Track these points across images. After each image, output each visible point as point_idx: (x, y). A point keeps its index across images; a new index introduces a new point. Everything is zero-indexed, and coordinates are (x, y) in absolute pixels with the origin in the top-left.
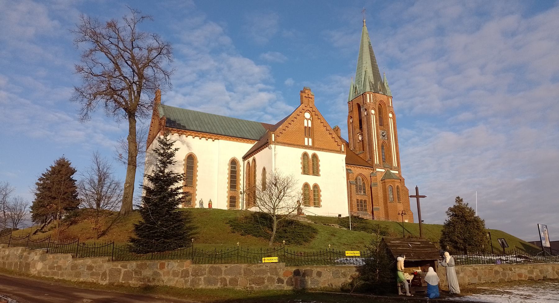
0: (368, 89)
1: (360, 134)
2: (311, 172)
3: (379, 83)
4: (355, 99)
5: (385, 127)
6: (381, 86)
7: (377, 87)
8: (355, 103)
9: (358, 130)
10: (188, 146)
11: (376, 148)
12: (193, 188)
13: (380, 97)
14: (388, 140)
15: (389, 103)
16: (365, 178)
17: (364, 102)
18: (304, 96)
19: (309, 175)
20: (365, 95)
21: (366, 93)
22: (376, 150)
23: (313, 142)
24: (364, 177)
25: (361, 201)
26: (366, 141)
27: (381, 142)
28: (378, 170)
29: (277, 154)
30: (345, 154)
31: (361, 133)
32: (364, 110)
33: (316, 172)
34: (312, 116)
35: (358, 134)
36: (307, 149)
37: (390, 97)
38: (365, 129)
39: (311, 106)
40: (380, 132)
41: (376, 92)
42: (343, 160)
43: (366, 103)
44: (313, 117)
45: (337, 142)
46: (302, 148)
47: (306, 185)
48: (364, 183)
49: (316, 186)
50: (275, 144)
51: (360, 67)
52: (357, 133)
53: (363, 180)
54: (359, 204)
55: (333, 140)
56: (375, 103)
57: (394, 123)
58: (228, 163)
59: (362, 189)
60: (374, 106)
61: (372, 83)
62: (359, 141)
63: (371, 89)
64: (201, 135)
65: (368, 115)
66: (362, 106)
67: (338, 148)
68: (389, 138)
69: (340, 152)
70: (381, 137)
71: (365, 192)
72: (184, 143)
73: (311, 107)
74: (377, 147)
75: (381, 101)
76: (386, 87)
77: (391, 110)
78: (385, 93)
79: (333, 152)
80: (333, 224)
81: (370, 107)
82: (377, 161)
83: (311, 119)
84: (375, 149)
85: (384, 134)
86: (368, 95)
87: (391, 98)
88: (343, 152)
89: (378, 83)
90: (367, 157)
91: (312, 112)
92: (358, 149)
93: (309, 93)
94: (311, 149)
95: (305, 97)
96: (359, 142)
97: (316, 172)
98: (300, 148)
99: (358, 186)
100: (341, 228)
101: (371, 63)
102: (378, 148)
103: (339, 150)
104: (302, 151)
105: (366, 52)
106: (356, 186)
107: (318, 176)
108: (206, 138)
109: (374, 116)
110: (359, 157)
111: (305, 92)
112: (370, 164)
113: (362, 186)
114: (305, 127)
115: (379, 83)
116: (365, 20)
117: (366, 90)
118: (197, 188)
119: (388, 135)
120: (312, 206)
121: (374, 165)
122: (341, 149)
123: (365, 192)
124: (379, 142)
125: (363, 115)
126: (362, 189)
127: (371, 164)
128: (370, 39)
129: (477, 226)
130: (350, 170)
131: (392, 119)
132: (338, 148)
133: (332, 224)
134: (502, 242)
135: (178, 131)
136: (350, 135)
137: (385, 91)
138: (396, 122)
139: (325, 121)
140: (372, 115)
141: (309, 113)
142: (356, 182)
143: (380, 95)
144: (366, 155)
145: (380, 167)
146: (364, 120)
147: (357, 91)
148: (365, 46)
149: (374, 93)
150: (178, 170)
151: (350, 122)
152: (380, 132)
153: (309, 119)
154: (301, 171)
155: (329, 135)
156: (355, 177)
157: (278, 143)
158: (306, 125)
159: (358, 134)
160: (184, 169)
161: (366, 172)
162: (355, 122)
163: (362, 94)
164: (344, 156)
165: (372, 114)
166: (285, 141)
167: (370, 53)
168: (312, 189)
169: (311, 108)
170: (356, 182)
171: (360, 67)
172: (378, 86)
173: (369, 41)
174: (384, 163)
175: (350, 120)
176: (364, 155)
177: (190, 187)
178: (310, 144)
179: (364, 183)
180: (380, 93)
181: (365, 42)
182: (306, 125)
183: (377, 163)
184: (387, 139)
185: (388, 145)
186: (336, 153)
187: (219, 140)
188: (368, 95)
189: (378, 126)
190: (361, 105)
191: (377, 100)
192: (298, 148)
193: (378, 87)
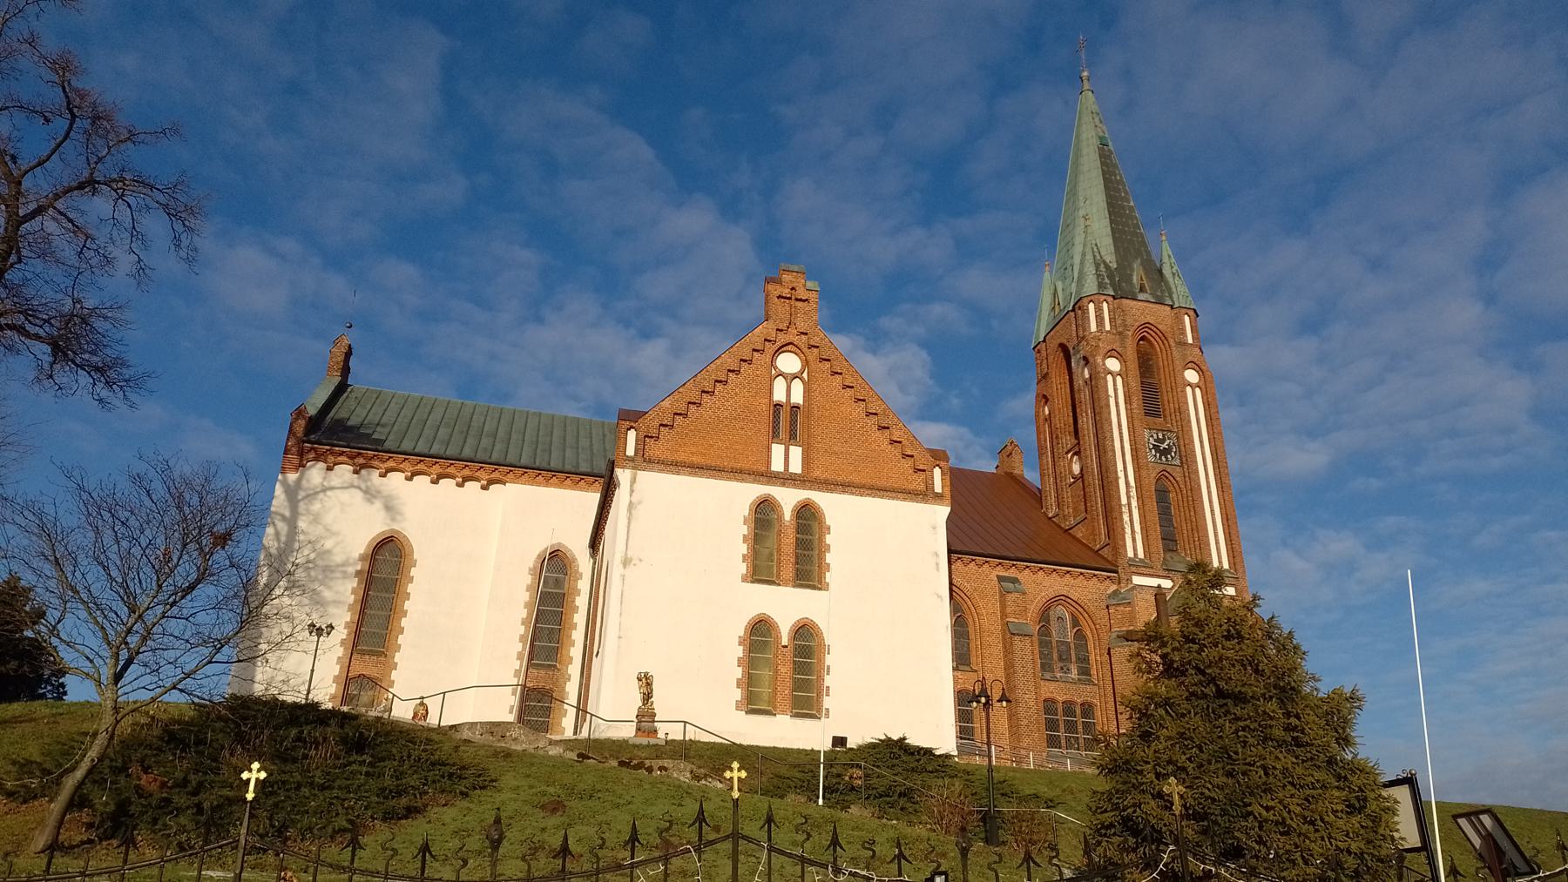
0: (1091, 286)
1: (1075, 454)
2: (788, 571)
3: (1137, 265)
4: (1052, 333)
5: (1168, 419)
6: (1145, 274)
7: (1129, 279)
8: (1053, 344)
9: (1068, 441)
10: (389, 508)
11: (1129, 497)
12: (382, 659)
13: (1141, 310)
14: (1182, 466)
15: (1183, 333)
16: (1086, 615)
17: (1081, 334)
18: (777, 293)
19: (779, 585)
20: (1080, 308)
21: (1085, 300)
22: (1129, 504)
23: (806, 461)
24: (1080, 609)
25: (1069, 708)
26: (1094, 479)
27: (1151, 476)
28: (1137, 580)
29: (640, 503)
30: (948, 502)
31: (1077, 449)
32: (1082, 362)
33: (808, 571)
34: (806, 363)
35: (1069, 455)
36: (774, 484)
37: (1184, 311)
38: (1088, 430)
39: (802, 326)
40: (1149, 438)
41: (1122, 292)
42: (934, 528)
43: (1083, 338)
44: (813, 366)
45: (912, 456)
46: (754, 481)
47: (760, 629)
48: (1080, 635)
49: (805, 632)
50: (634, 468)
51: (1069, 221)
52: (1065, 450)
53: (1075, 622)
54: (1061, 717)
55: (896, 451)
56: (1120, 333)
57: (1208, 405)
58: (531, 566)
59: (1073, 659)
60: (1118, 344)
61: (1107, 266)
62: (1072, 480)
63: (1101, 285)
64: (436, 469)
65: (1096, 384)
66: (1074, 348)
67: (917, 483)
68: (1187, 460)
69: (925, 495)
70: (1151, 456)
71: (1085, 671)
72: (375, 497)
73: (802, 330)
74: (1133, 493)
75: (1147, 325)
76: (1170, 280)
77: (1190, 359)
78: (1162, 297)
79: (894, 494)
80: (666, 763)
81: (1097, 346)
82: (1134, 545)
83: (805, 375)
84: (1124, 500)
85: (1165, 446)
86: (1091, 306)
87: (1191, 313)
88: (938, 498)
89: (1135, 266)
90: (1100, 534)
91: (805, 350)
92: (1071, 510)
93: (794, 285)
94: (795, 487)
95: (779, 297)
96: (1074, 483)
97: (808, 571)
98: (743, 480)
99: (1054, 645)
100: (697, 778)
101: (1108, 203)
102: (1140, 498)
103: (922, 487)
104: (752, 491)
105: (1089, 171)
106: (1044, 644)
107: (820, 589)
108: (453, 477)
109: (1119, 379)
110: (1074, 537)
111: (779, 282)
112: (1108, 561)
113: (1072, 645)
114: (778, 405)
115: (1137, 265)
116: (1085, 74)
117: (1085, 290)
118: (398, 657)
119: (1182, 448)
120: (783, 712)
121: (1120, 561)
122: (929, 485)
123: (1085, 671)
124: (1144, 473)
125: (1079, 382)
126: (1073, 659)
127: (1110, 558)
128: (1104, 127)
129: (1288, 728)
130: (1015, 581)
131: (1198, 390)
132: (917, 483)
133: (660, 763)
134: (1487, 837)
135: (352, 457)
136: (1045, 461)
137: (1162, 291)
138: (1214, 399)
139: (860, 381)
140: (1109, 378)
141: (796, 354)
142: (1045, 631)
143: (1140, 303)
144: (1094, 527)
145: (1151, 572)
146: (1084, 396)
147: (1059, 304)
148: (1085, 151)
149: (1114, 297)
150: (337, 592)
151: (1042, 417)
152: (1149, 438)
153: (795, 377)
154: (743, 568)
155: (878, 433)
156: (1034, 609)
157: (650, 461)
158: (779, 395)
159: (1067, 453)
160: (354, 591)
161: (1086, 589)
162: (1057, 413)
163: (1073, 310)
164: (942, 512)
165: (1110, 373)
166: (681, 457)
167: (1103, 170)
168: (785, 641)
169: (803, 336)
170: (1045, 631)
171: (1069, 221)
172: (1132, 275)
173: (1101, 134)
174: (1169, 555)
175: (1044, 410)
176: (1087, 530)
177: (371, 653)
178: (796, 467)
179: (1080, 635)
180: (1141, 296)
181: (1088, 139)
182: (779, 395)
183: (1136, 554)
184: (1178, 462)
185: (1182, 486)
186: (905, 499)
187: (504, 483)
188: (1091, 306)
189: (1135, 416)
190: (1071, 349)
191: (1129, 321)
192: (737, 480)
193: (1132, 280)
